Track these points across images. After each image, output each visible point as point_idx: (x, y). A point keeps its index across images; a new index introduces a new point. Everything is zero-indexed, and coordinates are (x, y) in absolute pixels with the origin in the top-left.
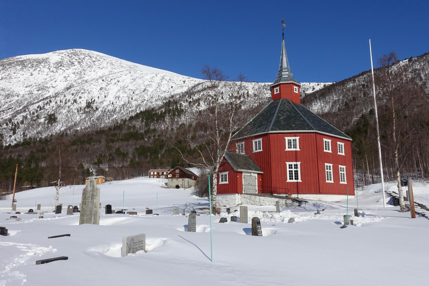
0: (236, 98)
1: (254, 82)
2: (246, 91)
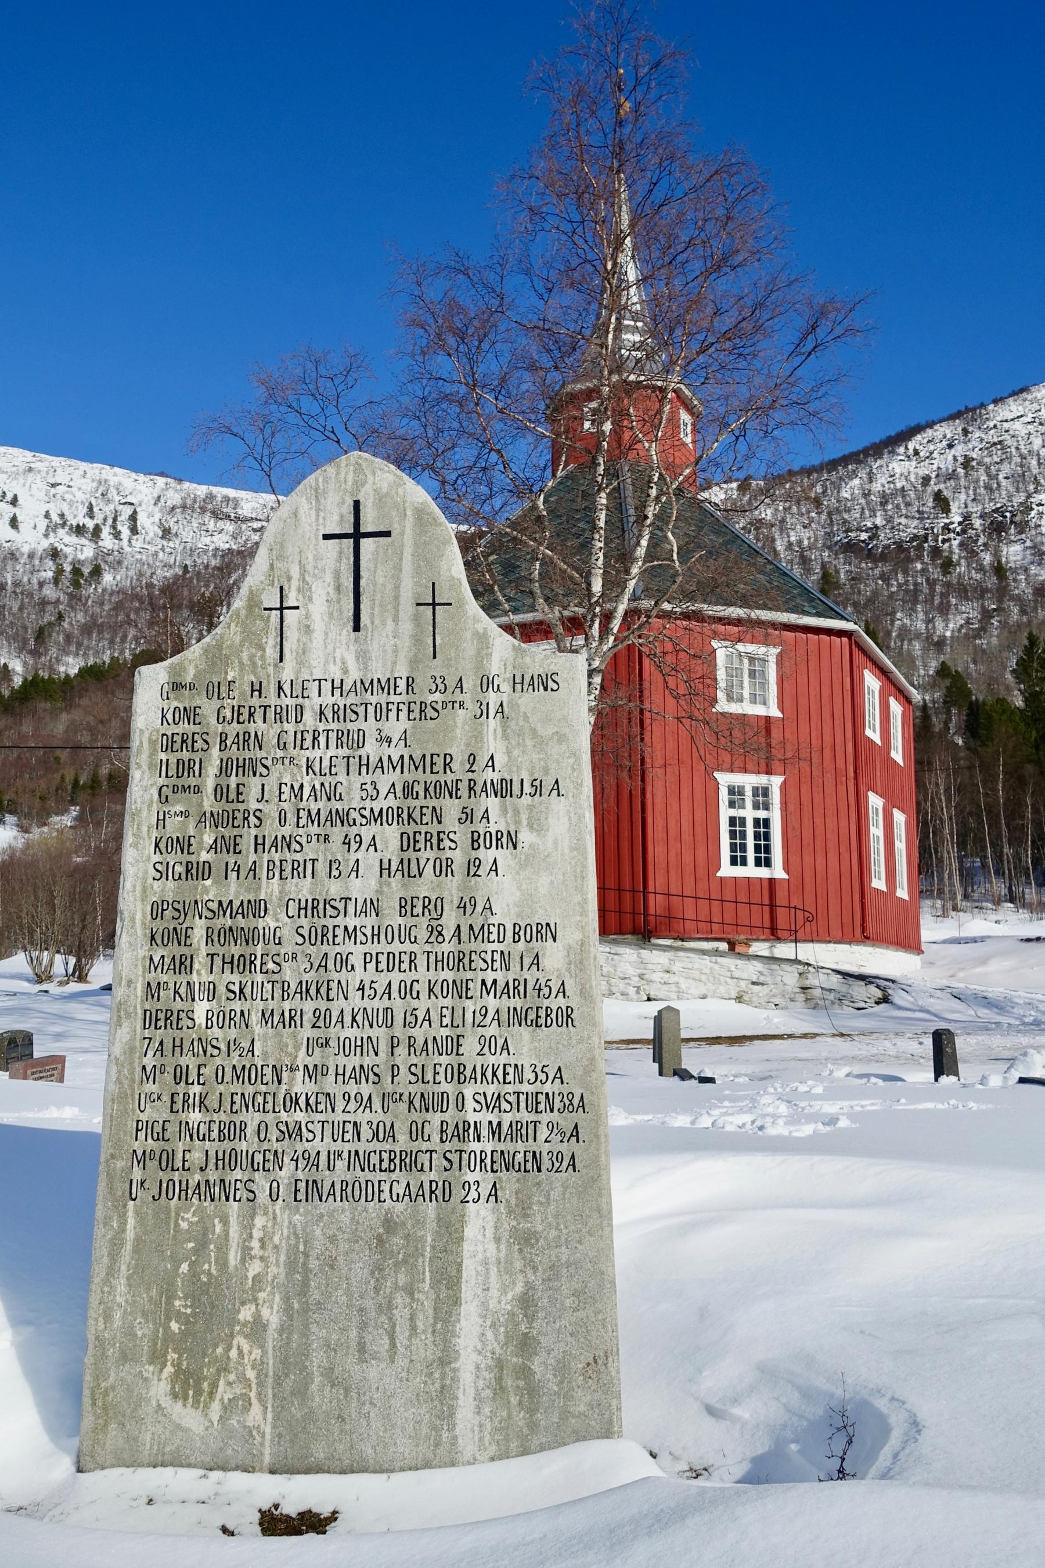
0: (79, 530)
1: (162, 474)
2: (128, 511)
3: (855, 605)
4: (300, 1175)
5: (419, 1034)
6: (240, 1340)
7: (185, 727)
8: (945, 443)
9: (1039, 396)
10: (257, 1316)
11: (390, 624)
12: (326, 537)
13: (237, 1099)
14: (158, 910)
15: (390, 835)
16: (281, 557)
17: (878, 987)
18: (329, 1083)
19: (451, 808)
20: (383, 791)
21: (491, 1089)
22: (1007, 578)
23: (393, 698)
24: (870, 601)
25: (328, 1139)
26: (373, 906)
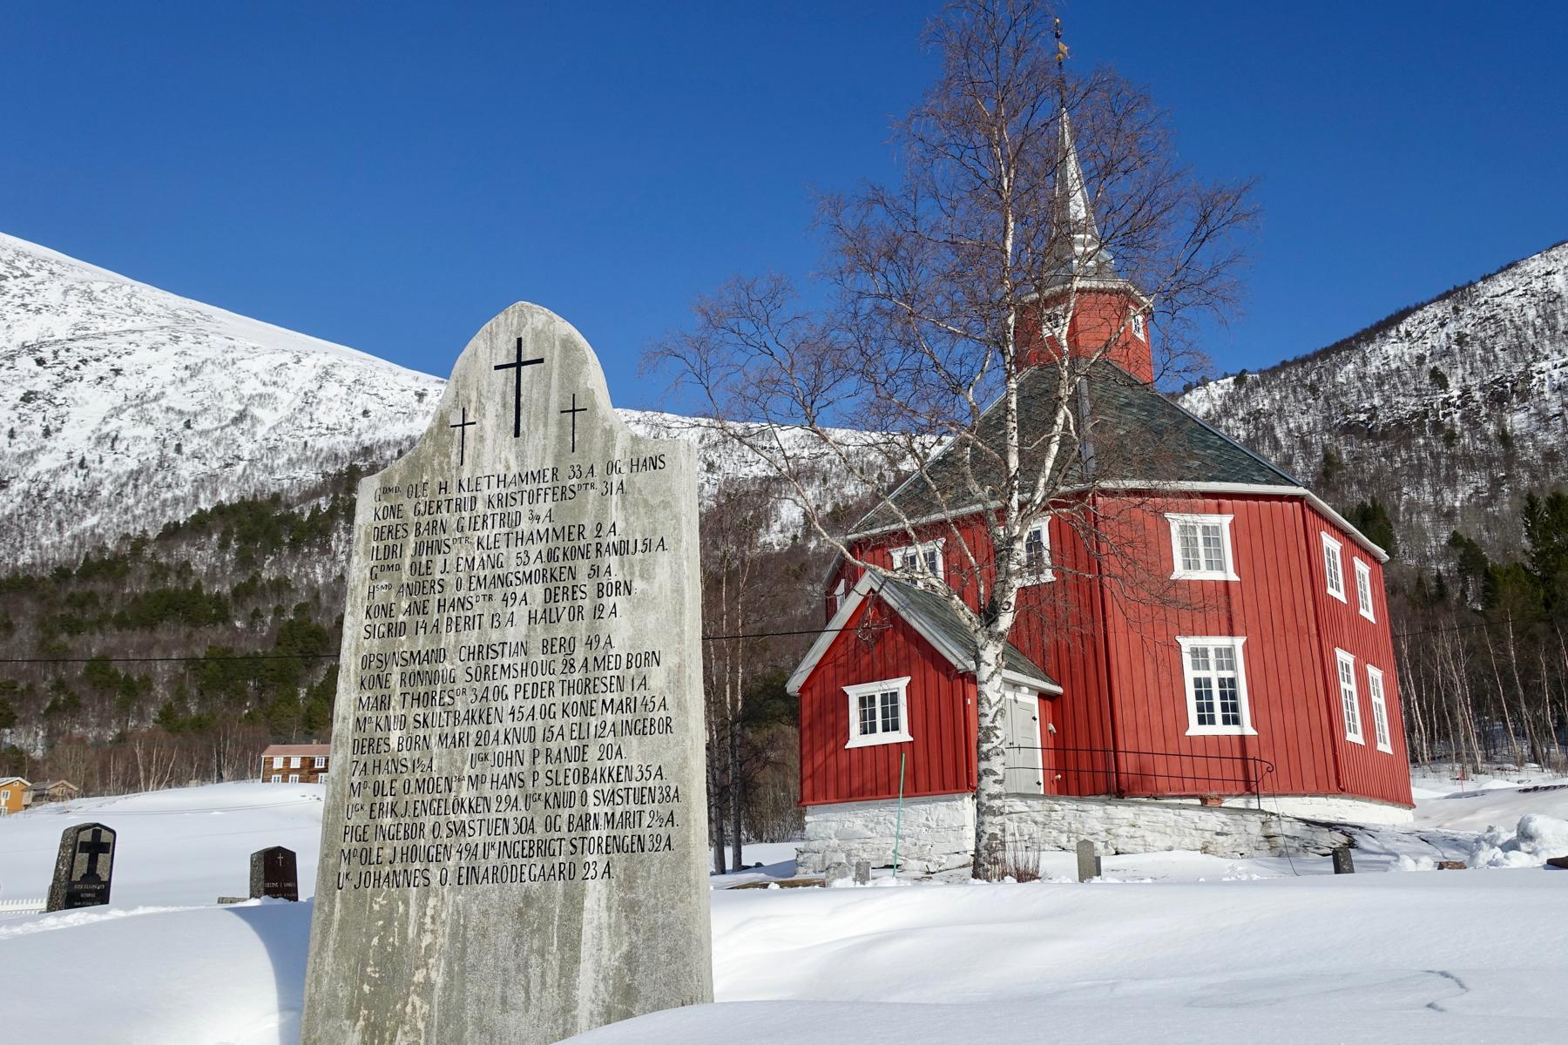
3: (1359, 483)
4: (463, 863)
5: (554, 746)
6: (414, 998)
7: (391, 521)
8: (1436, 323)
9: (1528, 269)
10: (427, 978)
12: (497, 368)
13: (419, 805)
14: (366, 662)
15: (537, 591)
16: (464, 386)
17: (1343, 833)
18: (487, 790)
19: (583, 566)
20: (533, 557)
21: (607, 787)
22: (1513, 446)
24: (1375, 478)
25: (484, 833)
26: (523, 648)
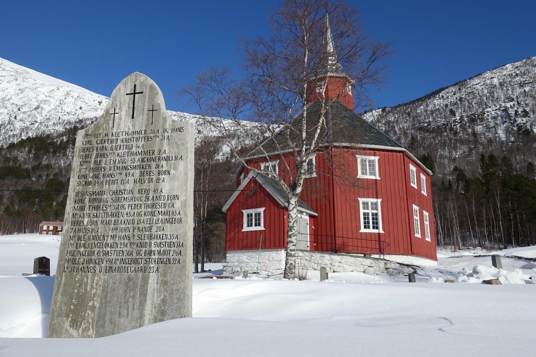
3: (423, 147)
6: (89, 311)
7: (88, 146)
10: (93, 304)
11: (141, 116)
12: (127, 94)
13: (93, 244)
14: (77, 194)
15: (137, 172)
16: (115, 100)
17: (412, 268)
19: (153, 164)
20: (136, 160)
21: (159, 241)
22: (477, 137)
23: (141, 136)
26: (132, 192)
